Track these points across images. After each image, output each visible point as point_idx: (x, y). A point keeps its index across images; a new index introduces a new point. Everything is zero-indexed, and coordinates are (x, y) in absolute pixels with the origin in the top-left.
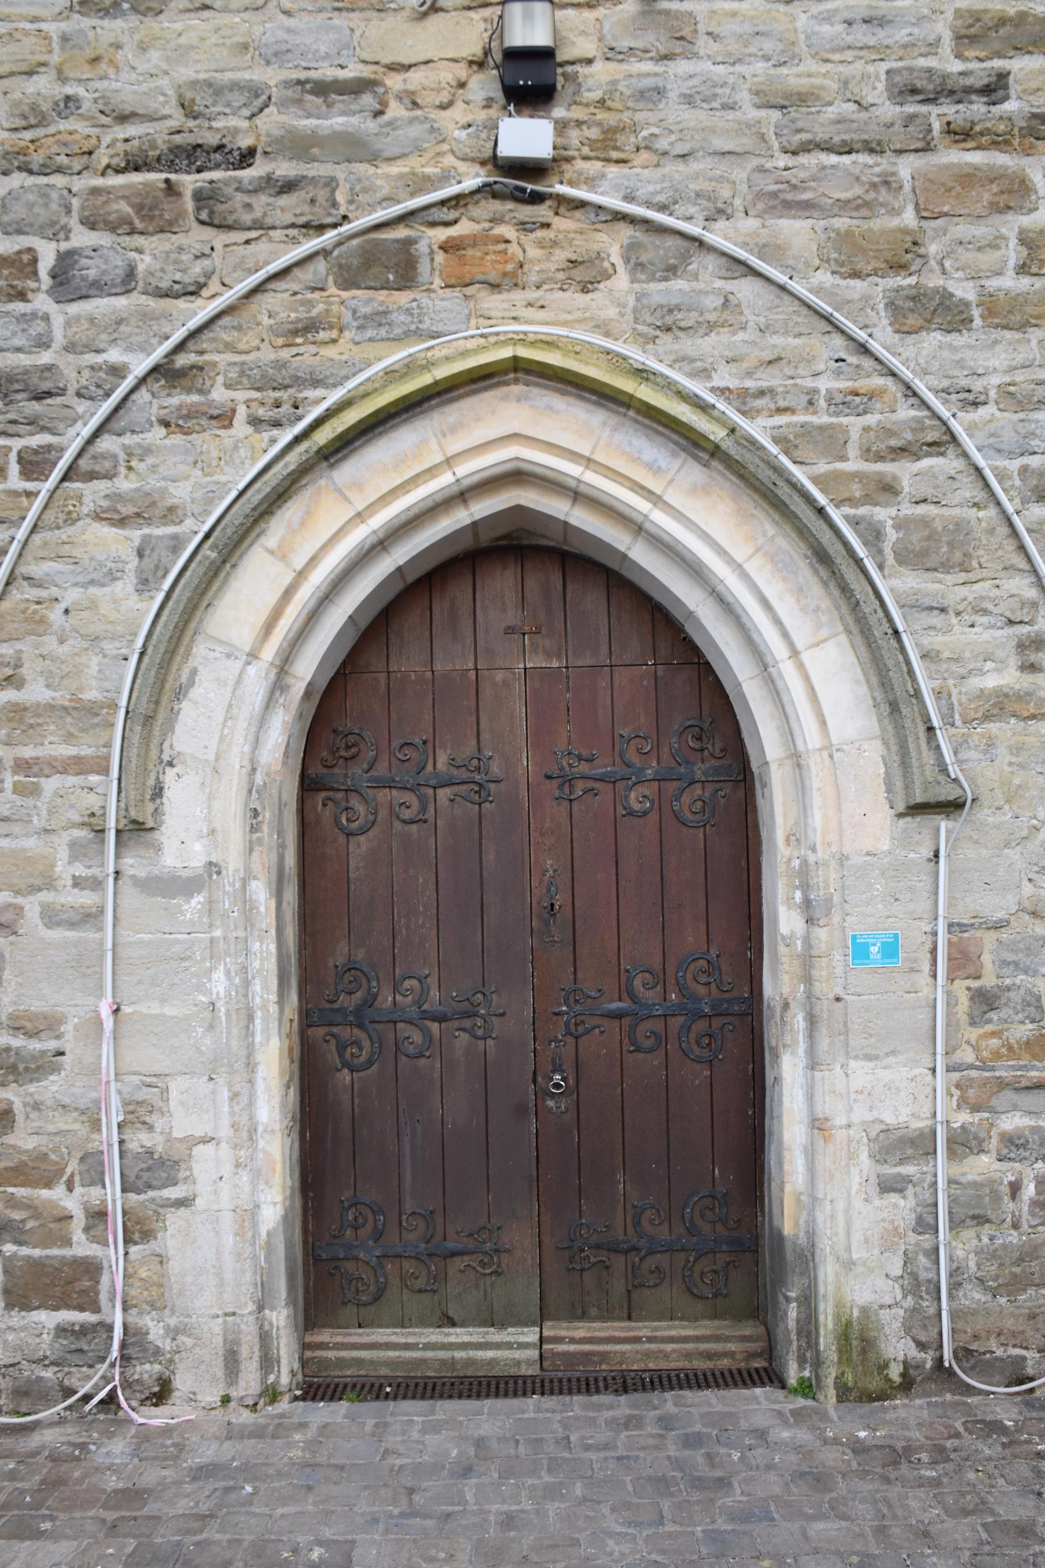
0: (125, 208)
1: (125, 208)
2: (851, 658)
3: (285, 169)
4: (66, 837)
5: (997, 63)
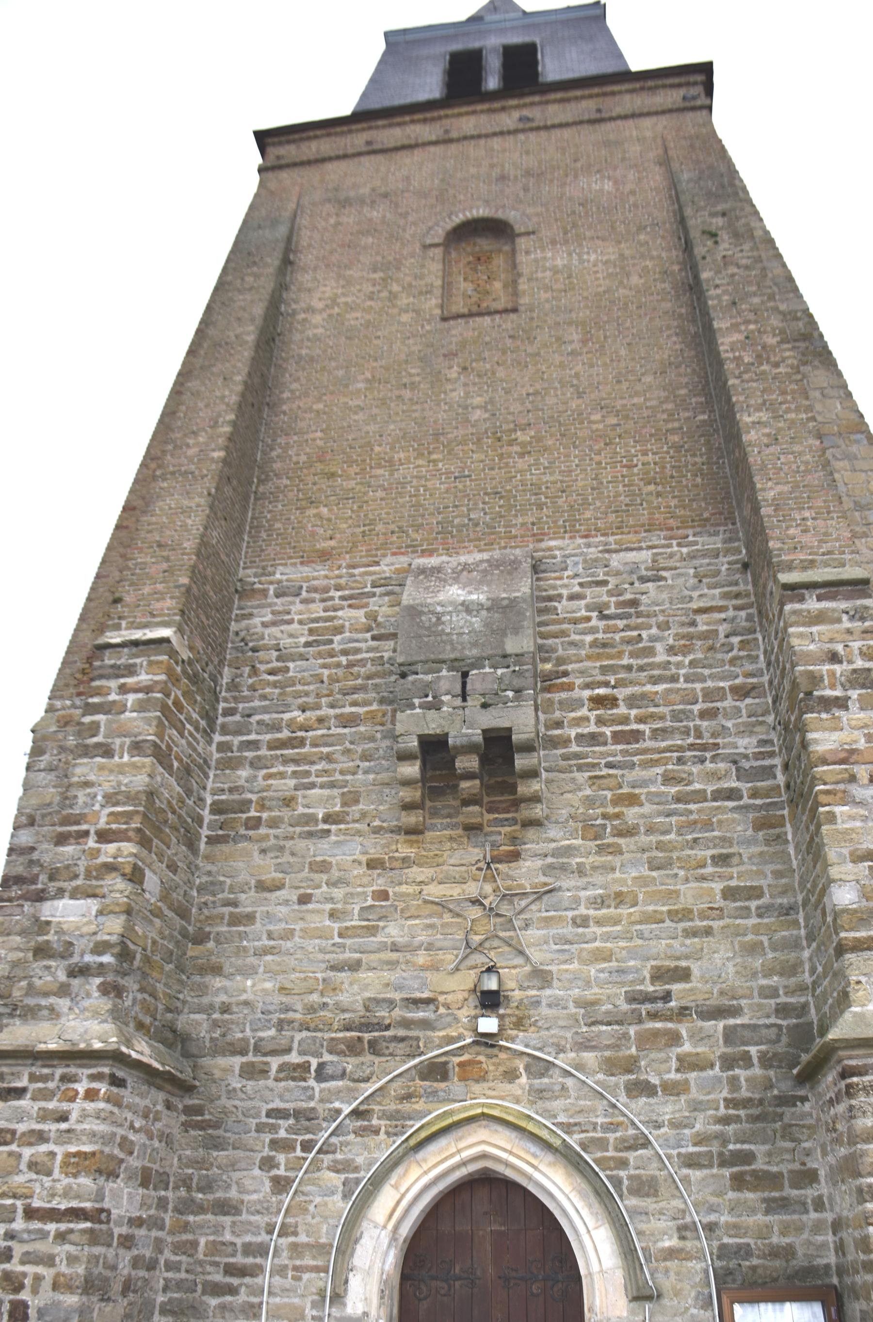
0: (343, 1047)
1: (343, 1047)
2: (610, 1234)
3: (401, 1033)
4: (310, 1298)
5: (667, 987)
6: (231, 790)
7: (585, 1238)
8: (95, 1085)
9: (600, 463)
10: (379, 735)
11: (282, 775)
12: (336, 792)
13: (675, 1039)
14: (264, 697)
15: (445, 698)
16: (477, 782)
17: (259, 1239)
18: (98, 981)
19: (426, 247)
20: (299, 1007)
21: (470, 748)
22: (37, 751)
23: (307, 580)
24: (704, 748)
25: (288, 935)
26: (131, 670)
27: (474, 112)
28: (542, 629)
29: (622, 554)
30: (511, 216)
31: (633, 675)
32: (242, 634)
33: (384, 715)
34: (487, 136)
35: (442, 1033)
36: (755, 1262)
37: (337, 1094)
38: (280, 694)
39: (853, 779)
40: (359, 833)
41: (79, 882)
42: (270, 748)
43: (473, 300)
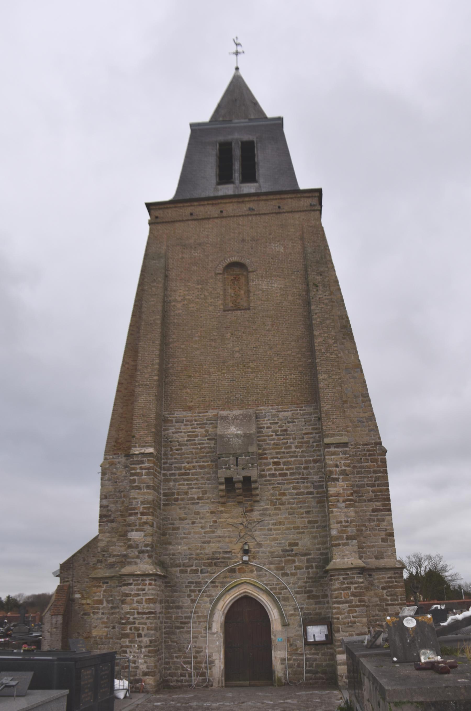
0: (207, 565)
1: (207, 565)
3: (223, 560)
6: (169, 489)
7: (271, 612)
8: (151, 582)
9: (276, 378)
10: (211, 472)
11: (183, 485)
12: (200, 490)
13: (294, 561)
14: (175, 459)
15: (232, 466)
16: (241, 490)
17: (188, 615)
18: (147, 554)
19: (217, 274)
20: (194, 554)
21: (239, 482)
22: (103, 473)
23: (185, 417)
24: (304, 479)
25: (189, 533)
26: (142, 462)
27: (231, 202)
28: (259, 438)
29: (283, 413)
30: (247, 261)
31: (285, 455)
32: (166, 436)
33: (213, 466)
34: (237, 216)
35: (233, 560)
36: (312, 616)
37: (206, 577)
38: (181, 458)
39: (338, 501)
40: (208, 503)
41: (137, 527)
42: (179, 476)
43: (234, 298)
